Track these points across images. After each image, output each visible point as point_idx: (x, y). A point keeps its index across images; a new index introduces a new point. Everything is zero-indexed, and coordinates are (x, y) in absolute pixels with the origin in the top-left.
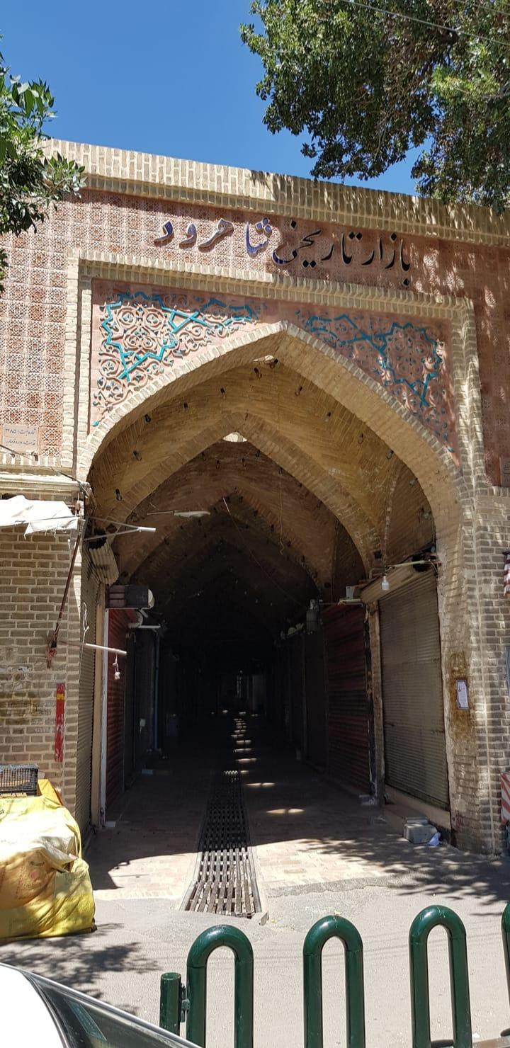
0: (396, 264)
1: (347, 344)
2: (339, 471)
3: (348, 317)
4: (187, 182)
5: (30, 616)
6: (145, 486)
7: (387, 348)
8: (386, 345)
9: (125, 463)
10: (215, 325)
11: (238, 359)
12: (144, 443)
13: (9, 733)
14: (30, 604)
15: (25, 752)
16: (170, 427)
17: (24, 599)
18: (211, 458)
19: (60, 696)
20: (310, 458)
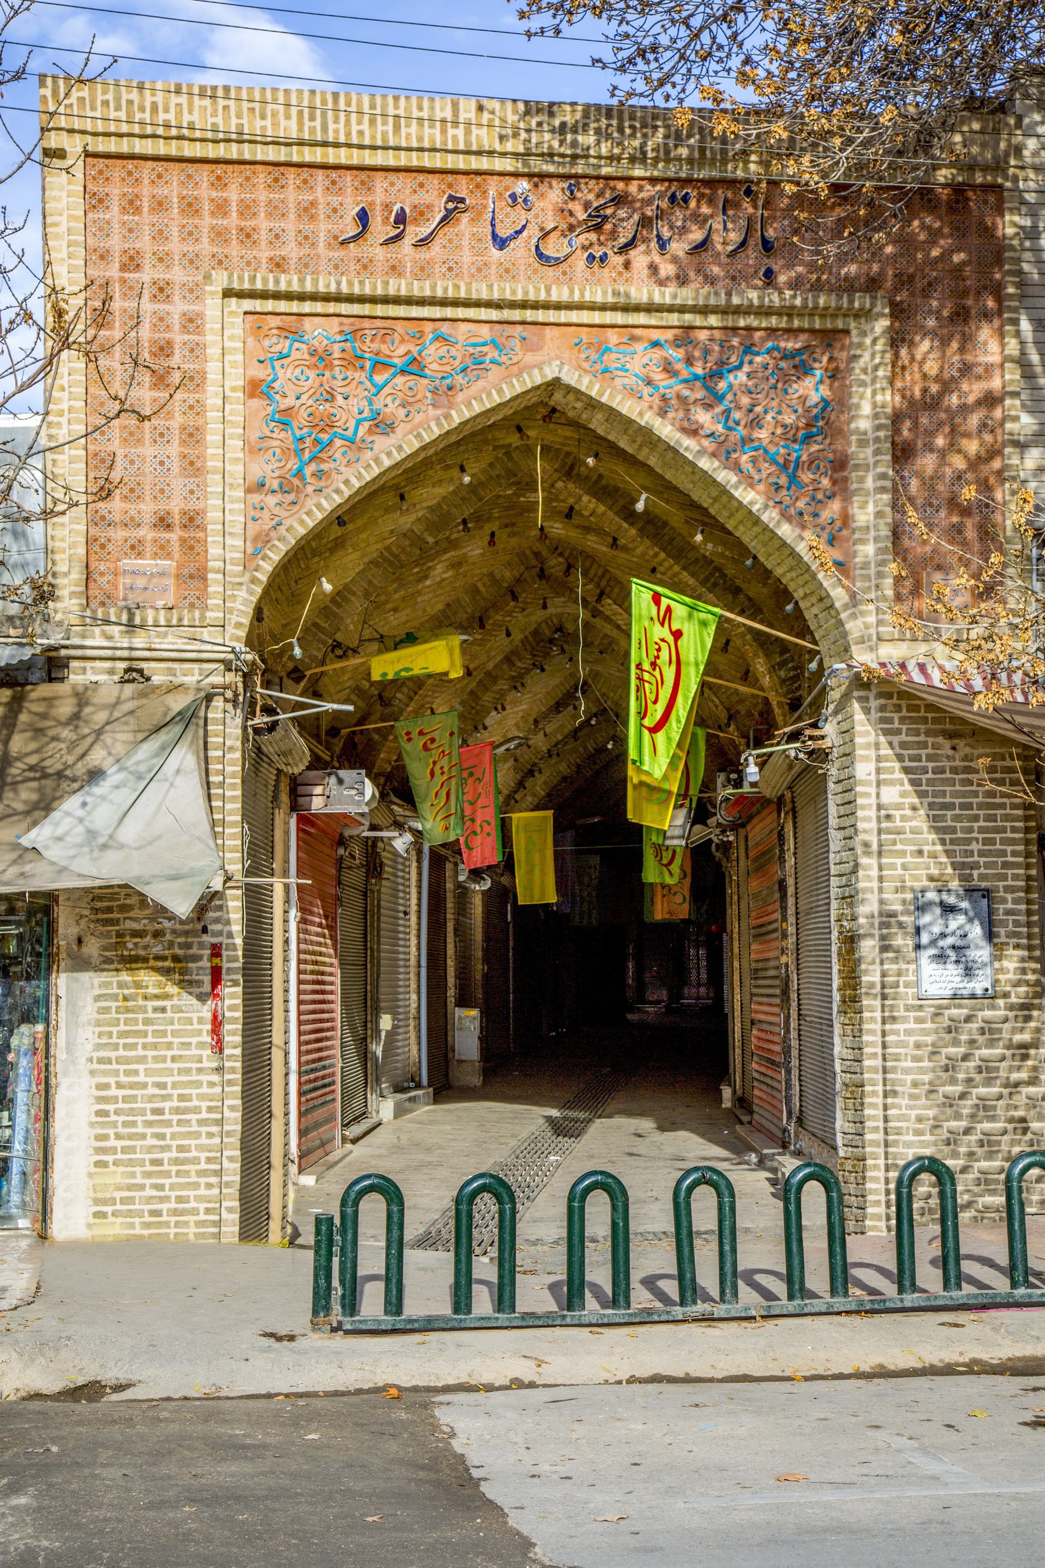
0: (751, 242)
4: (391, 135)
6: (354, 594)
9: (316, 559)
10: (440, 375)
13: (146, 1012)
15: (170, 1039)
19: (217, 960)
20: (666, 524)
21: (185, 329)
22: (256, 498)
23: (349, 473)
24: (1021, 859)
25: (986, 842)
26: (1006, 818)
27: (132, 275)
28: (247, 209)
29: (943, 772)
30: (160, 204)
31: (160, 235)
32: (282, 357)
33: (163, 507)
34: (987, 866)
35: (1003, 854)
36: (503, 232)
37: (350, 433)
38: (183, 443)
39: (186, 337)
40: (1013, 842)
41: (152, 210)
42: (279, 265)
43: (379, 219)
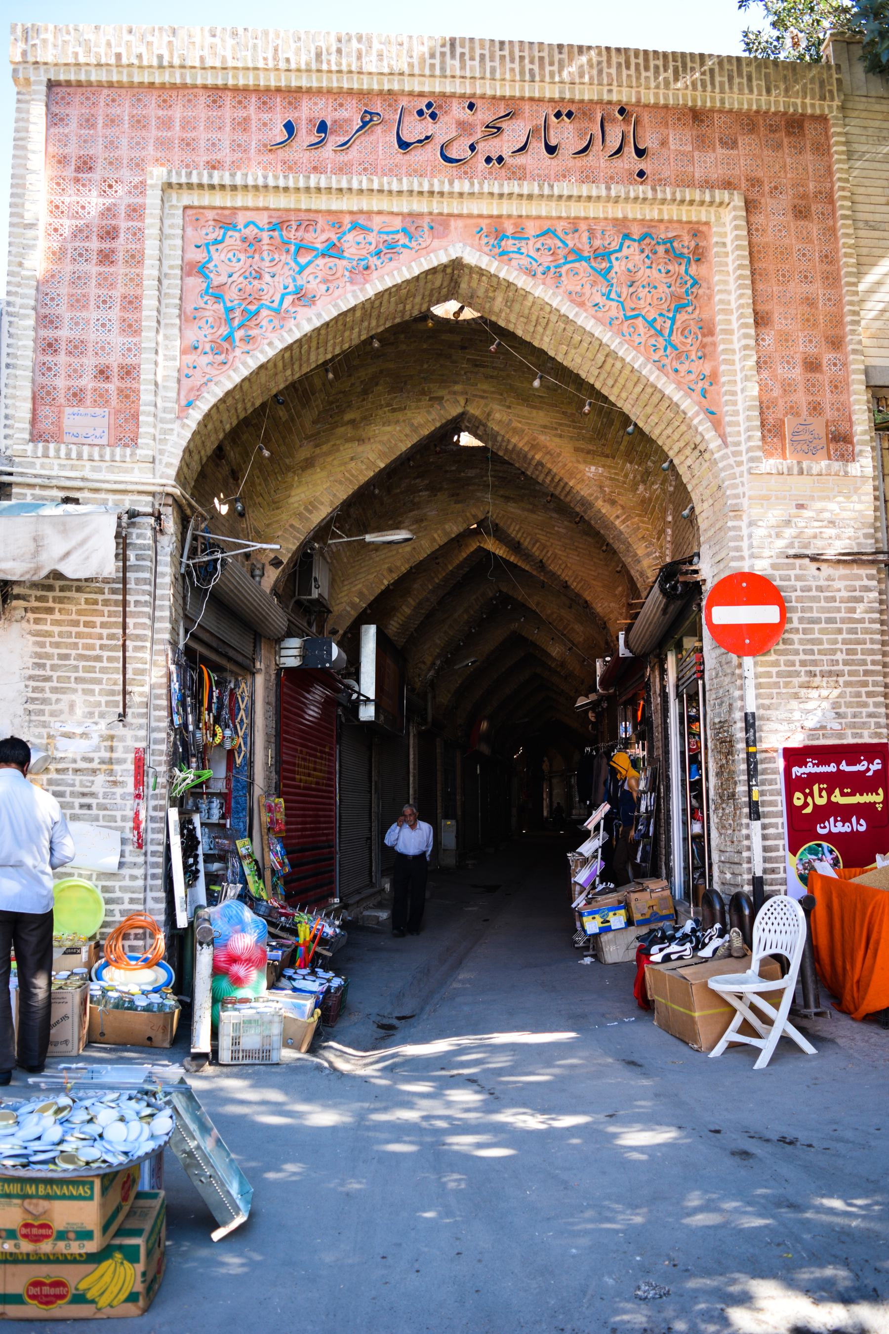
0: (626, 149)
1: (552, 270)
2: (600, 470)
3: (554, 232)
5: (98, 658)
7: (613, 272)
8: (611, 267)
11: (401, 307)
12: (316, 446)
13: (72, 808)
14: (98, 643)
16: (352, 422)
17: (90, 636)
18: (446, 472)
21: (129, 217)
22: (190, 359)
23: (273, 337)
24: (879, 668)
25: (849, 652)
26: (866, 631)
27: (84, 176)
28: (186, 124)
29: (810, 590)
30: (112, 121)
31: (111, 145)
32: (216, 242)
33: (103, 361)
34: (851, 674)
35: (864, 663)
36: (406, 138)
37: (275, 305)
38: (123, 308)
39: (130, 224)
40: (872, 652)
41: (105, 125)
42: (213, 166)
43: (304, 131)
